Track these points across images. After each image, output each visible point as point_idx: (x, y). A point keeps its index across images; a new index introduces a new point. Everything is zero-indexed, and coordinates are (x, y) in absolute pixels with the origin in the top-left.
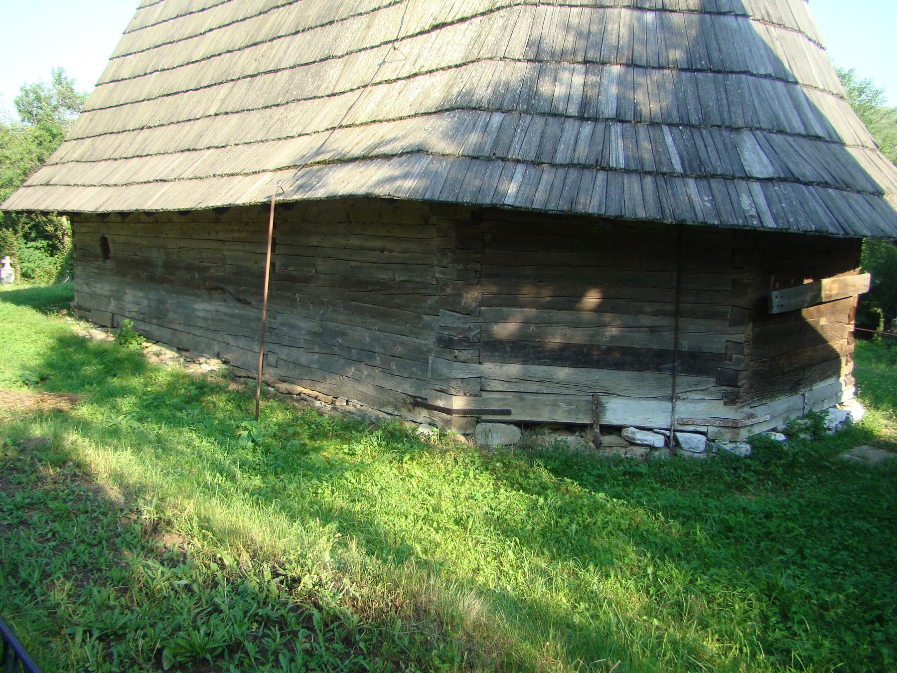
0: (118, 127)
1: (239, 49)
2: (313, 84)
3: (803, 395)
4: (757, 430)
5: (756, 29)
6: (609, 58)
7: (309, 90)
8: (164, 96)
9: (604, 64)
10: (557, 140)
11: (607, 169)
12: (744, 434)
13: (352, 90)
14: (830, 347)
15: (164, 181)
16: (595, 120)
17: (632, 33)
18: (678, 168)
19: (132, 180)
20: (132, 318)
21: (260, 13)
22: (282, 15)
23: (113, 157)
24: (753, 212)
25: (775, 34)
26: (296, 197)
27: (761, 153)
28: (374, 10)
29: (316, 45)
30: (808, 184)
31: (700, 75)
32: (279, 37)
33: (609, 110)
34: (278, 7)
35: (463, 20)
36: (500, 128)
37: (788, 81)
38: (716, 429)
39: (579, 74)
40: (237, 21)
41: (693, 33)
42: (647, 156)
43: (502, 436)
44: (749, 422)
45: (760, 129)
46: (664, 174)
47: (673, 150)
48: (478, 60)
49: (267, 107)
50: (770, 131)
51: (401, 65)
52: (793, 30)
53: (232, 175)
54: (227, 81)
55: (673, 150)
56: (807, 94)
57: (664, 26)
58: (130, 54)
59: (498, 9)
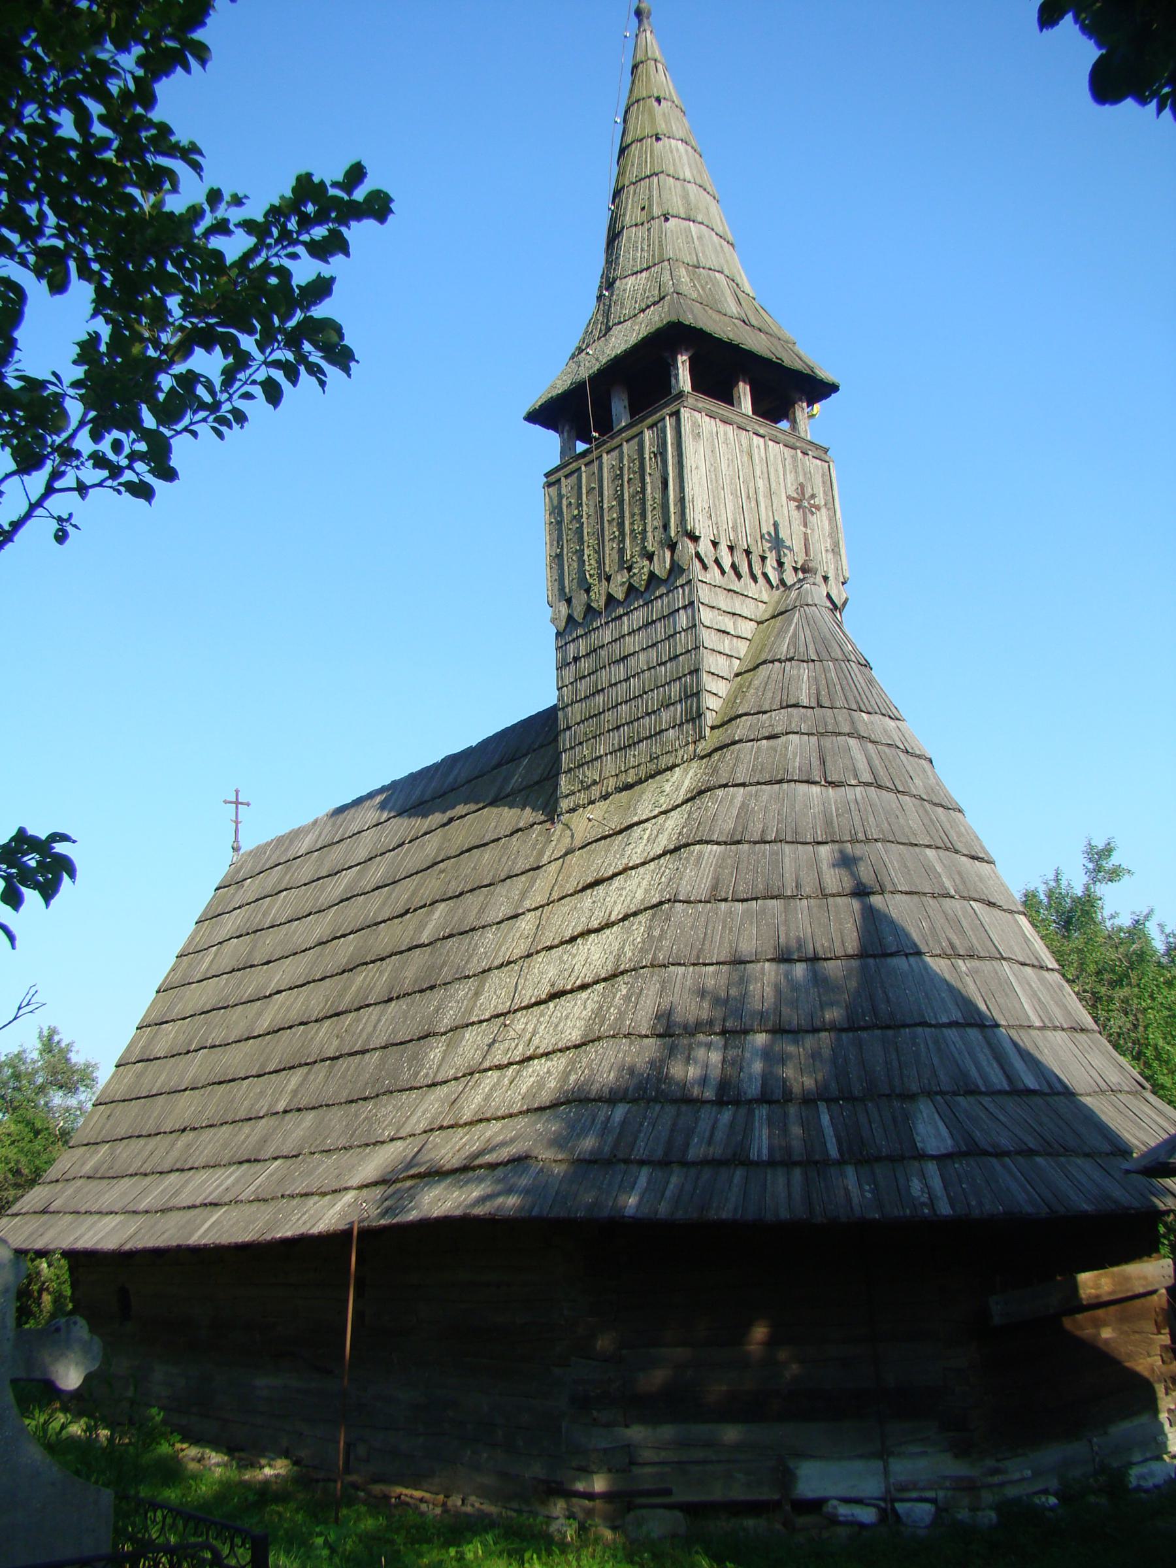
0: (150, 1127)
1: (316, 1021)
2: (409, 1070)
3: (1090, 1441)
4: (1011, 1492)
5: (935, 968)
6: (752, 1025)
7: (405, 1077)
8: (214, 1084)
9: (746, 1032)
10: (690, 1133)
11: (747, 1163)
12: (987, 1497)
13: (456, 1079)
14: (1127, 1369)
15: (216, 1205)
16: (737, 1103)
17: (778, 990)
18: (834, 1152)
19: (171, 1204)
20: (161, 1408)
21: (344, 972)
22: (371, 974)
23: (142, 1170)
24: (925, 1198)
25: (964, 969)
26: (383, 1222)
27: (941, 1124)
28: (484, 972)
29: (413, 1018)
30: (1001, 1154)
31: (864, 1035)
32: (368, 1006)
33: (753, 1090)
34: (366, 964)
35: (584, 987)
36: (624, 1123)
37: (983, 1024)
38: (950, 1493)
39: (716, 1049)
40: (314, 981)
41: (853, 984)
42: (797, 1144)
43: (659, 1524)
44: (996, 1479)
45: (941, 1093)
46: (816, 1163)
47: (829, 1131)
48: (599, 1039)
49: (352, 1102)
50: (955, 1094)
51: (513, 1045)
52: (992, 958)
53: (306, 1195)
54: (300, 1065)
55: (829, 1131)
56: (1016, 1038)
57: (818, 980)
58: (167, 1022)
59: (622, 973)
